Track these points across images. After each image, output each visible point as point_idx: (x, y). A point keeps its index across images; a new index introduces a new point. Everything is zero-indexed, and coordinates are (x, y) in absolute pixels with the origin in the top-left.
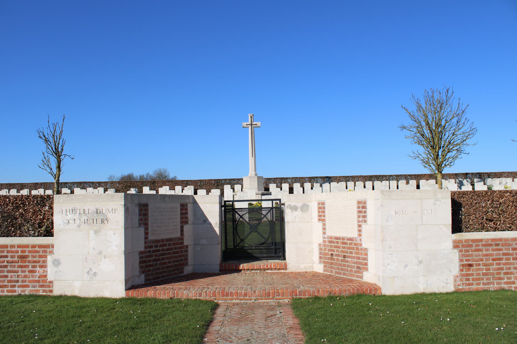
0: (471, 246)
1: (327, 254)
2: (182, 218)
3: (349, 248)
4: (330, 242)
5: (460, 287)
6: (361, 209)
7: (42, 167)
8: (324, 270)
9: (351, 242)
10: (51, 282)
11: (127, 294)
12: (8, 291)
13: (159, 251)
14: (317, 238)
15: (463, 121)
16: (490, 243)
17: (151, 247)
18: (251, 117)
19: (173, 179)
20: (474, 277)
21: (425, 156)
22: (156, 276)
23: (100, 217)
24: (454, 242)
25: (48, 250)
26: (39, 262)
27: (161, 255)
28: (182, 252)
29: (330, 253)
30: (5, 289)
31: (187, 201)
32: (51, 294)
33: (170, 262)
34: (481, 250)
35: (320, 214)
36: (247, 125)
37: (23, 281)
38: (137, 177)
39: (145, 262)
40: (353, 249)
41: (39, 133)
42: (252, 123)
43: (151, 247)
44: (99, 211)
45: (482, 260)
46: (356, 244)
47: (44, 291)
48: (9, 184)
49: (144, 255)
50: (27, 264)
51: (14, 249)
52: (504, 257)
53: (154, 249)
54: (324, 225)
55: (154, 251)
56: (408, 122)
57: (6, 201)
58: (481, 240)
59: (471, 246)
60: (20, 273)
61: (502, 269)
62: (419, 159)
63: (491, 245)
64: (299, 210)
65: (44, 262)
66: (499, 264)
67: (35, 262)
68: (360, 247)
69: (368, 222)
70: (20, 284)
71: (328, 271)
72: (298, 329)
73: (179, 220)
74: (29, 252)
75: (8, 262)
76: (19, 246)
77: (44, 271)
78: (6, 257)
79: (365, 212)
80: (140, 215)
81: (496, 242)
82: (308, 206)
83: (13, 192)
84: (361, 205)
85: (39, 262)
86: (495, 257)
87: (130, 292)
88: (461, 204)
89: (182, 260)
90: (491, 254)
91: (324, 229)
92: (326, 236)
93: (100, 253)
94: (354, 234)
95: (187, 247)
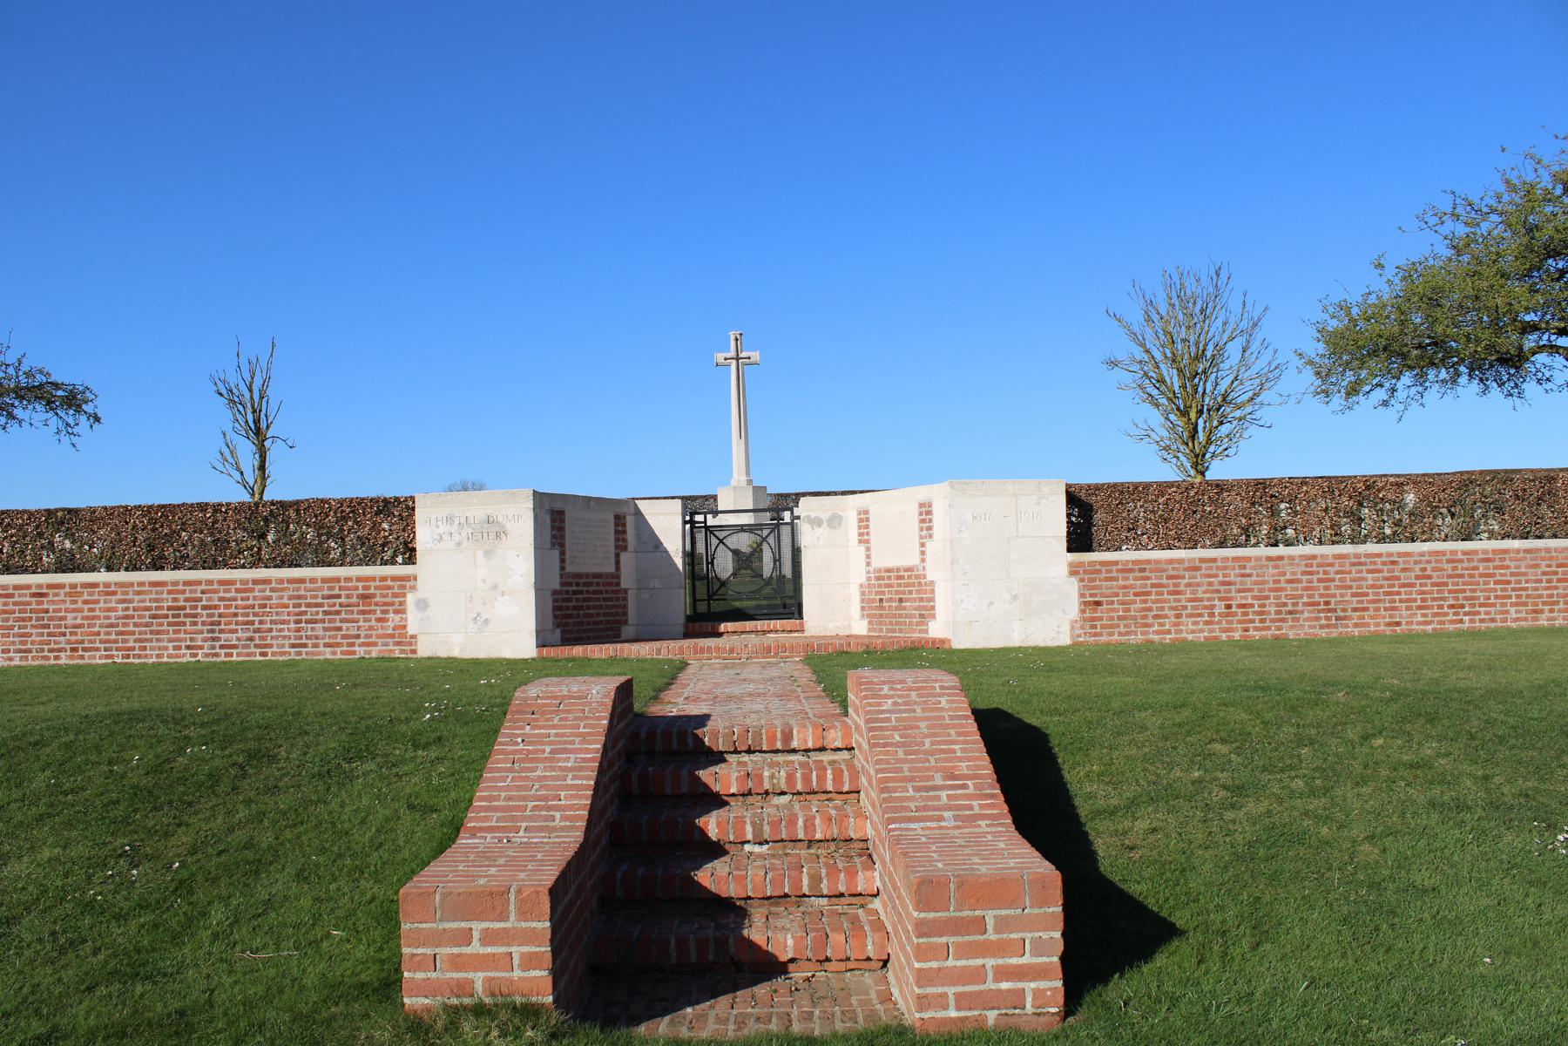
0: (1099, 572)
1: (873, 601)
2: (617, 540)
3: (908, 585)
4: (878, 578)
6: (924, 517)
7: (221, 467)
8: (870, 630)
9: (909, 573)
10: (413, 637)
11: (540, 653)
12: (343, 653)
13: (581, 592)
14: (857, 575)
15: (1254, 347)
16: (1131, 567)
17: (570, 584)
18: (737, 340)
20: (1105, 622)
21: (1165, 433)
22: (577, 635)
24: (1071, 565)
25: (408, 584)
26: (392, 604)
27: (585, 600)
28: (617, 599)
29: (878, 597)
30: (339, 650)
31: (625, 510)
32: (414, 656)
33: (598, 615)
34: (1115, 579)
35: (862, 531)
36: (726, 359)
37: (367, 636)
39: (560, 608)
41: (216, 384)
43: (570, 584)
44: (491, 519)
45: (1117, 595)
46: (917, 577)
47: (402, 651)
49: (559, 597)
50: (373, 608)
52: (1154, 590)
53: (574, 588)
54: (868, 549)
55: (575, 593)
56: (1126, 349)
57: (323, 508)
59: (1099, 572)
60: (361, 623)
61: (1150, 609)
62: (1148, 440)
63: (1131, 571)
64: (825, 524)
65: (401, 603)
66: (1145, 601)
67: (385, 604)
68: (923, 581)
69: (935, 537)
70: (362, 640)
71: (874, 630)
73: (612, 543)
74: (376, 588)
75: (341, 605)
76: (359, 579)
77: (402, 618)
78: (339, 596)
79: (930, 521)
80: (553, 528)
81: (1141, 567)
82: (841, 517)
84: (924, 509)
85: (392, 604)
86: (1138, 590)
88: (1091, 506)
89: (617, 614)
90: (1132, 585)
91: (868, 557)
92: (871, 569)
93: (495, 587)
94: (914, 560)
95: (626, 591)
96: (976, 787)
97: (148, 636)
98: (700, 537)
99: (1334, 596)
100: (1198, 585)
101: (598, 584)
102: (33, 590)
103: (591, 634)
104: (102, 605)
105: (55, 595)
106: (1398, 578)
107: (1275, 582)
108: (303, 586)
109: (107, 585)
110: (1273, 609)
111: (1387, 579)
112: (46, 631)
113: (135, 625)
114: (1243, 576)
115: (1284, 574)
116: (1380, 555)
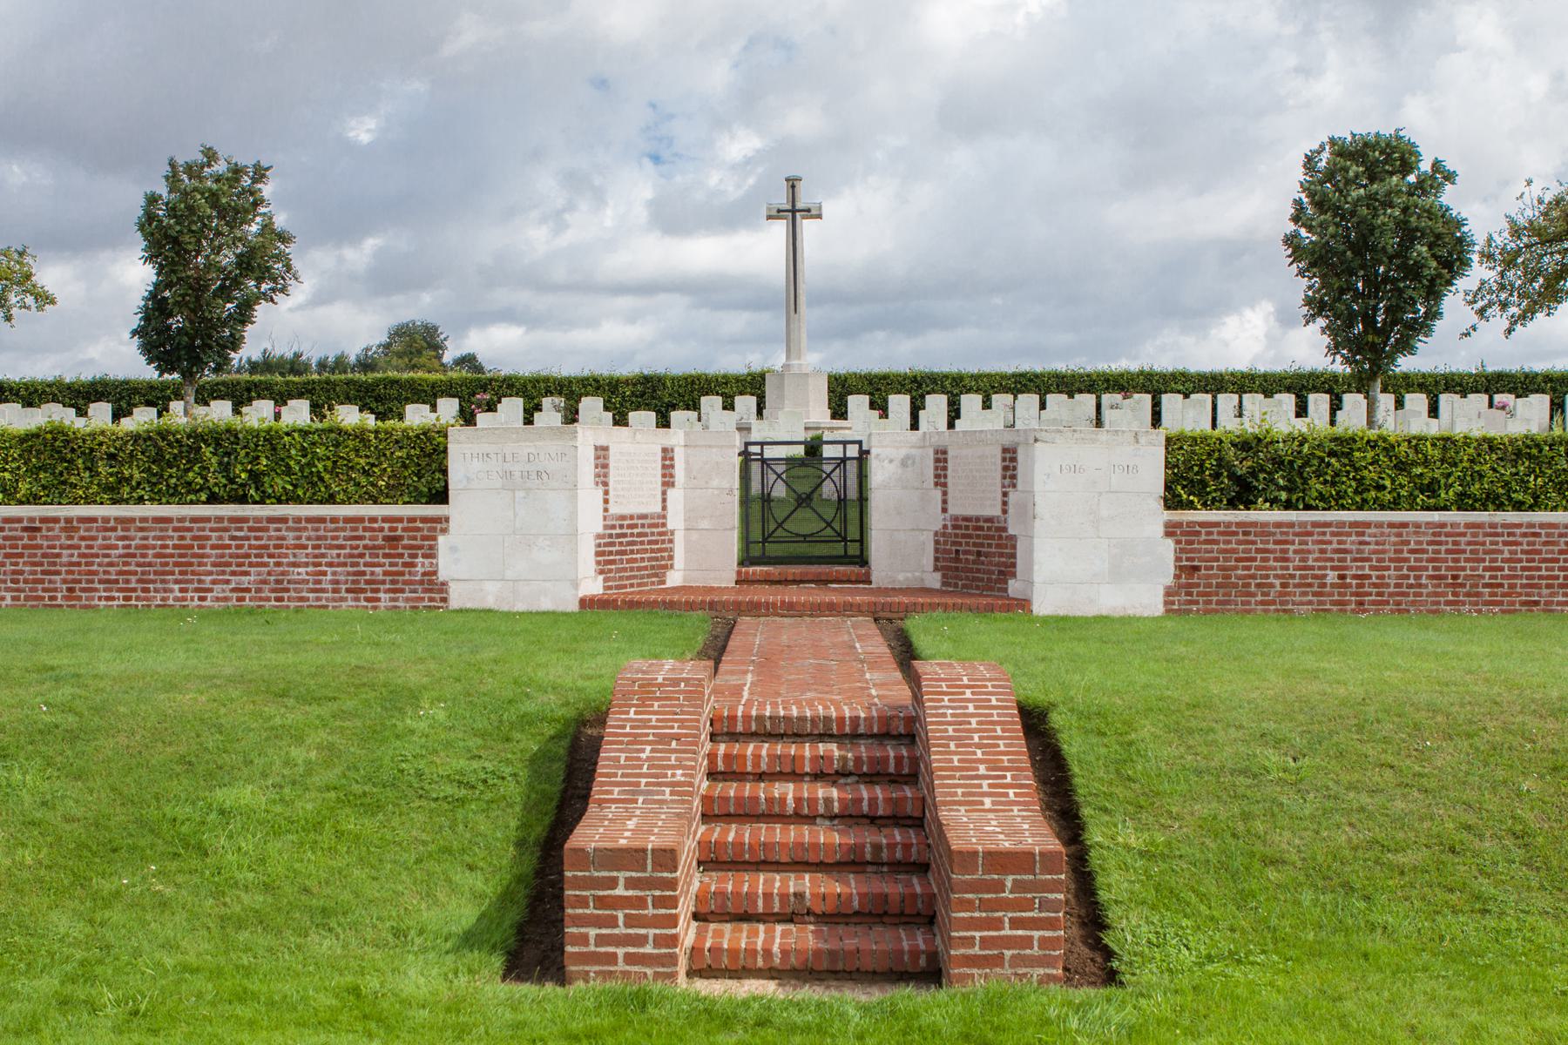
1: (949, 552)
8: (944, 584)
10: (443, 584)
13: (624, 535)
17: (613, 527)
28: (663, 542)
33: (643, 559)
40: (992, 537)
43: (613, 527)
45: (1217, 560)
49: (602, 541)
51: (375, 525)
52: (1259, 556)
53: (618, 531)
55: (619, 536)
58: (1217, 524)
59: (1198, 533)
65: (431, 547)
68: (1004, 534)
70: (388, 586)
71: (949, 585)
72: (717, 76)
73: (659, 480)
76: (385, 519)
83: (298, 413)
89: (663, 558)
95: (672, 533)
96: (1013, 777)
97: (152, 577)
98: (755, 468)
99: (1464, 569)
100: (1309, 552)
101: (643, 526)
102: (25, 524)
103: (635, 581)
104: (100, 541)
105: (49, 529)
106: (1539, 552)
107: (1396, 551)
108: (323, 526)
109: (106, 520)
110: (1393, 582)
111: (1526, 552)
112: (39, 569)
113: (138, 565)
114: (1361, 543)
115: (1408, 543)
116: (1519, 526)
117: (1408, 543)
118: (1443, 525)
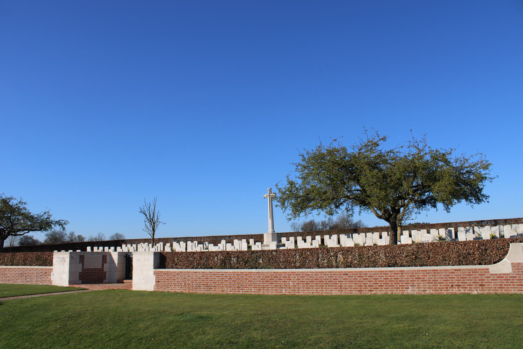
5: (156, 290)
10: (52, 281)
11: (69, 286)
19: (356, 224)
23: (64, 260)
24: (154, 272)
34: (162, 276)
36: (266, 196)
38: (319, 223)
42: (270, 195)
45: (162, 280)
48: (145, 239)
61: (169, 284)
63: (166, 274)
87: (70, 285)
106: (224, 279)
110: (195, 285)
116: (220, 272)
117: (197, 276)
118: (204, 272)
